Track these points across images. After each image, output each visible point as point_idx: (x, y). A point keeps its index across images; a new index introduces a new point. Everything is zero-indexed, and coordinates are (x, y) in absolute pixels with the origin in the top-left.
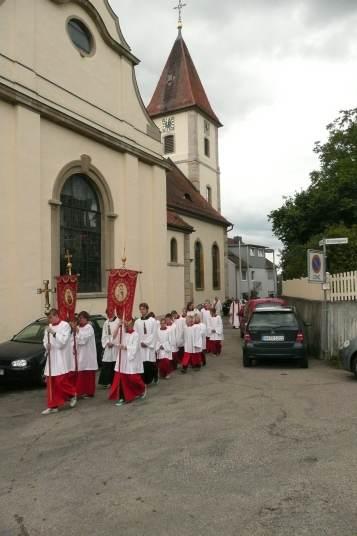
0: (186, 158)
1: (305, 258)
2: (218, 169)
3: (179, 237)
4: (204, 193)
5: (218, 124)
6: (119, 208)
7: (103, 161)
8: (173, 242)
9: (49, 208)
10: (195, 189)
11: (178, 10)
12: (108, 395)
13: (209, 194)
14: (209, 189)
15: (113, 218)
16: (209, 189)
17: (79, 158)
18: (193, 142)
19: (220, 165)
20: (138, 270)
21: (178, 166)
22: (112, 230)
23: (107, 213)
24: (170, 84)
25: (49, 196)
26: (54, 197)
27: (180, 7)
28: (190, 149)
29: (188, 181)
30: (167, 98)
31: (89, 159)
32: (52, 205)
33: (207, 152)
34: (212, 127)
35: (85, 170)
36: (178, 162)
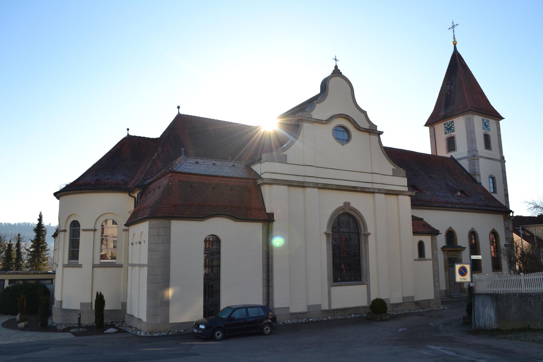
0: (466, 155)
1: (454, 267)
2: (503, 158)
3: (427, 240)
4: (486, 184)
5: (498, 117)
6: (370, 229)
7: (360, 203)
8: (421, 245)
9: (325, 235)
10: (475, 181)
11: (451, 30)
12: (45, 222)
13: (494, 183)
14: (493, 178)
15: (367, 235)
16: (493, 178)
17: (343, 205)
18: (471, 140)
19: (504, 154)
20: (417, 262)
21: (460, 162)
22: (366, 242)
23: (363, 232)
24: (449, 93)
25: (325, 229)
26: (327, 229)
27: (453, 27)
28: (468, 148)
29: (469, 175)
30: (447, 106)
31: (349, 203)
32: (327, 234)
33: (488, 146)
34: (492, 122)
35: (347, 210)
36: (460, 159)
